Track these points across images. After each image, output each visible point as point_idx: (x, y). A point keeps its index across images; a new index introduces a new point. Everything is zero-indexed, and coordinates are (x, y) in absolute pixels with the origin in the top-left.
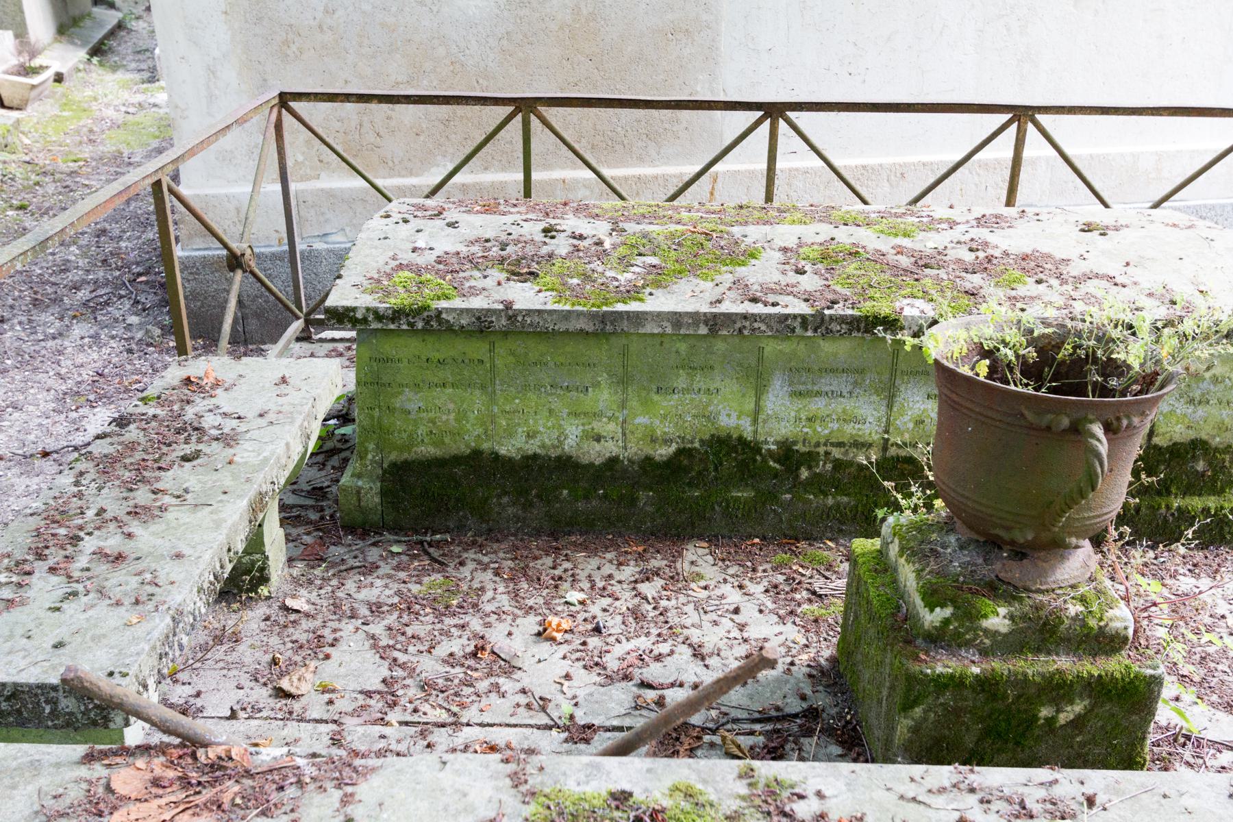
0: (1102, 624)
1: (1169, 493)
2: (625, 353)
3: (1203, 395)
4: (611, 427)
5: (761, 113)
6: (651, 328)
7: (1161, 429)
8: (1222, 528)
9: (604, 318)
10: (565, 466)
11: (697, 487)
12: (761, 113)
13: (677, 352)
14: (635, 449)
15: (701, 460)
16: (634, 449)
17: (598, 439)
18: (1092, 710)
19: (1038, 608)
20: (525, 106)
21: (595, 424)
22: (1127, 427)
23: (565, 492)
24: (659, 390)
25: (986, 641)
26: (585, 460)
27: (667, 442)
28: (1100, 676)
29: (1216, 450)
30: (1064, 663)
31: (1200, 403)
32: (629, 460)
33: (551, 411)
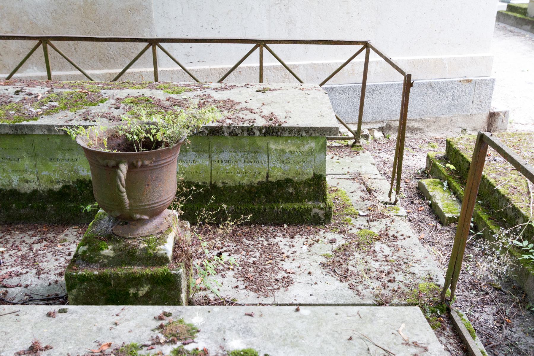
0: (155, 252)
1: (279, 202)
2: (32, 143)
3: (287, 159)
4: (32, 176)
5: (147, 43)
6: (38, 132)
7: (271, 174)
8: (302, 217)
9: (16, 128)
10: (14, 194)
11: (73, 202)
12: (147, 43)
13: (56, 143)
14: (44, 186)
15: (74, 190)
16: (44, 186)
17: (27, 182)
18: (153, 289)
19: (128, 245)
20: (44, 41)
21: (25, 175)
22: (142, 166)
23: (14, 205)
24: (50, 160)
25: (105, 260)
26: (23, 191)
27: (58, 182)
28: (151, 274)
29: (296, 183)
30: (137, 270)
31: (286, 163)
32: (42, 191)
33: (4, 170)
